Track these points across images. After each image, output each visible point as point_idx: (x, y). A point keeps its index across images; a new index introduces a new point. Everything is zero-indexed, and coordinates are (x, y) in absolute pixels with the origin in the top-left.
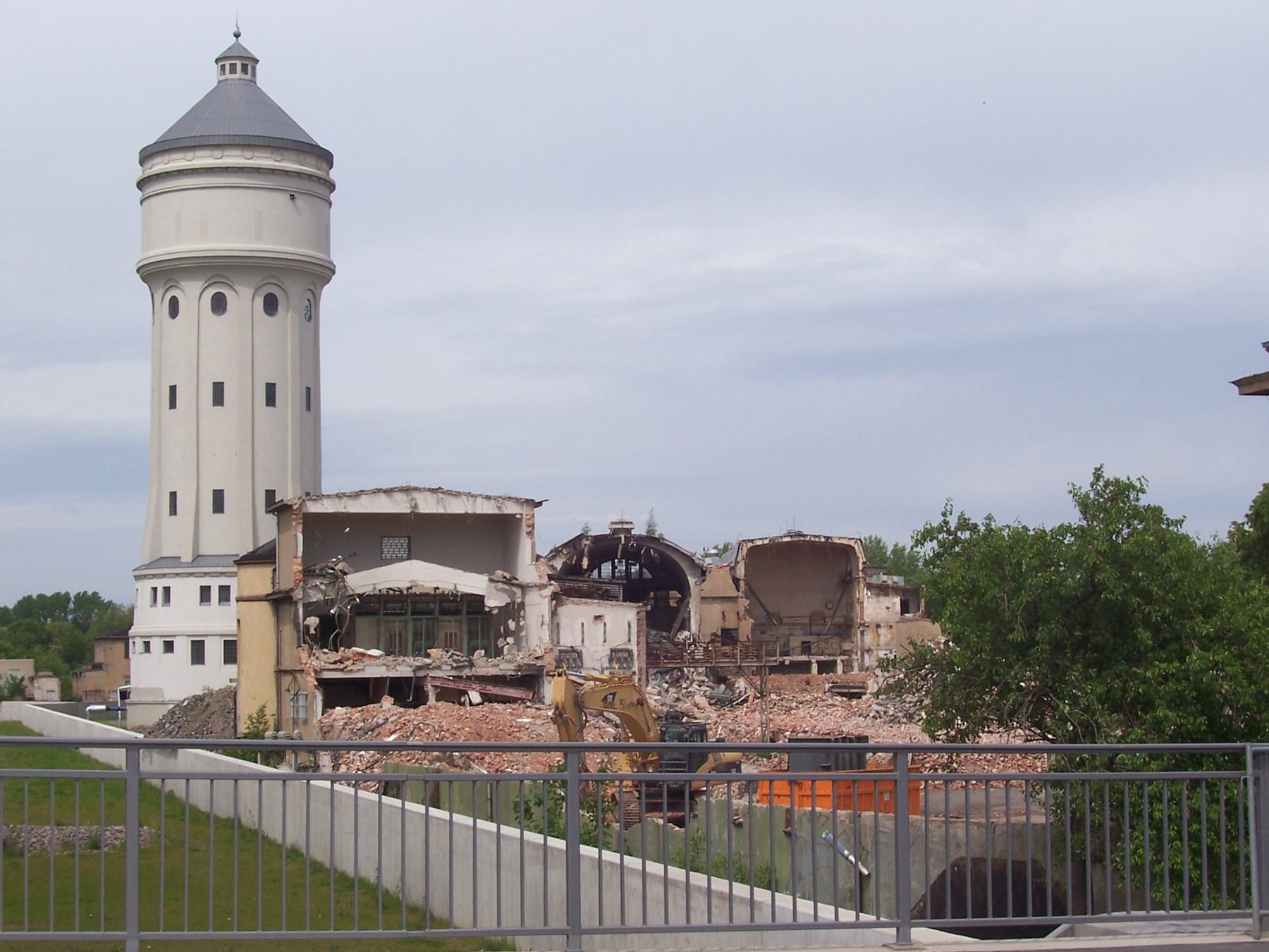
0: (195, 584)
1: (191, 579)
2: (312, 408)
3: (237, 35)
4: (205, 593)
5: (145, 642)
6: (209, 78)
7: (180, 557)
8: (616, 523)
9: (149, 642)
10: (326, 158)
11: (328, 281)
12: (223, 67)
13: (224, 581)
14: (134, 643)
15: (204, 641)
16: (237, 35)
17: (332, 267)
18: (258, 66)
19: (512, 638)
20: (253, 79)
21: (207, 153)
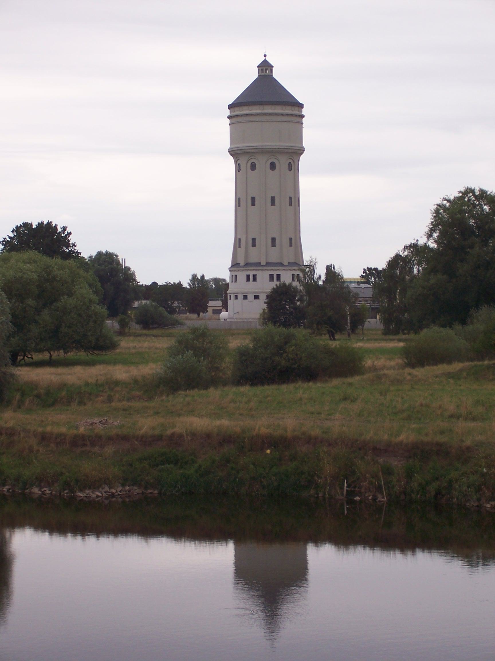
0: (267, 274)
1: (266, 271)
2: (288, 199)
3: (265, 56)
4: (248, 277)
5: (235, 296)
6: (254, 75)
7: (240, 264)
8: (9, 607)
9: (237, 296)
10: (301, 106)
11: (302, 154)
12: (262, 70)
13: (254, 273)
14: (230, 296)
15: (247, 295)
16: (265, 56)
17: (303, 149)
18: (274, 69)
19: (269, 453)
20: (271, 74)
21: (257, 107)
